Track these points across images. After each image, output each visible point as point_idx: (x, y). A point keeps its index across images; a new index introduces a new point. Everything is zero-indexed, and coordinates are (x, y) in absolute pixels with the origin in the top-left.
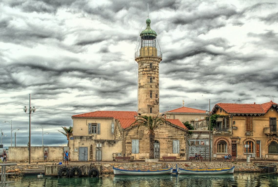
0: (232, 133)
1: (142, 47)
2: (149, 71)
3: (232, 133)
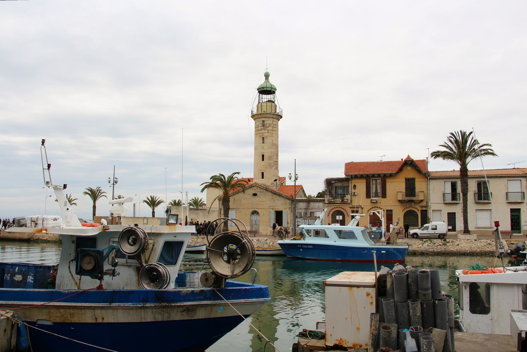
0: (351, 201)
1: (259, 103)
2: (261, 130)
3: (351, 201)
